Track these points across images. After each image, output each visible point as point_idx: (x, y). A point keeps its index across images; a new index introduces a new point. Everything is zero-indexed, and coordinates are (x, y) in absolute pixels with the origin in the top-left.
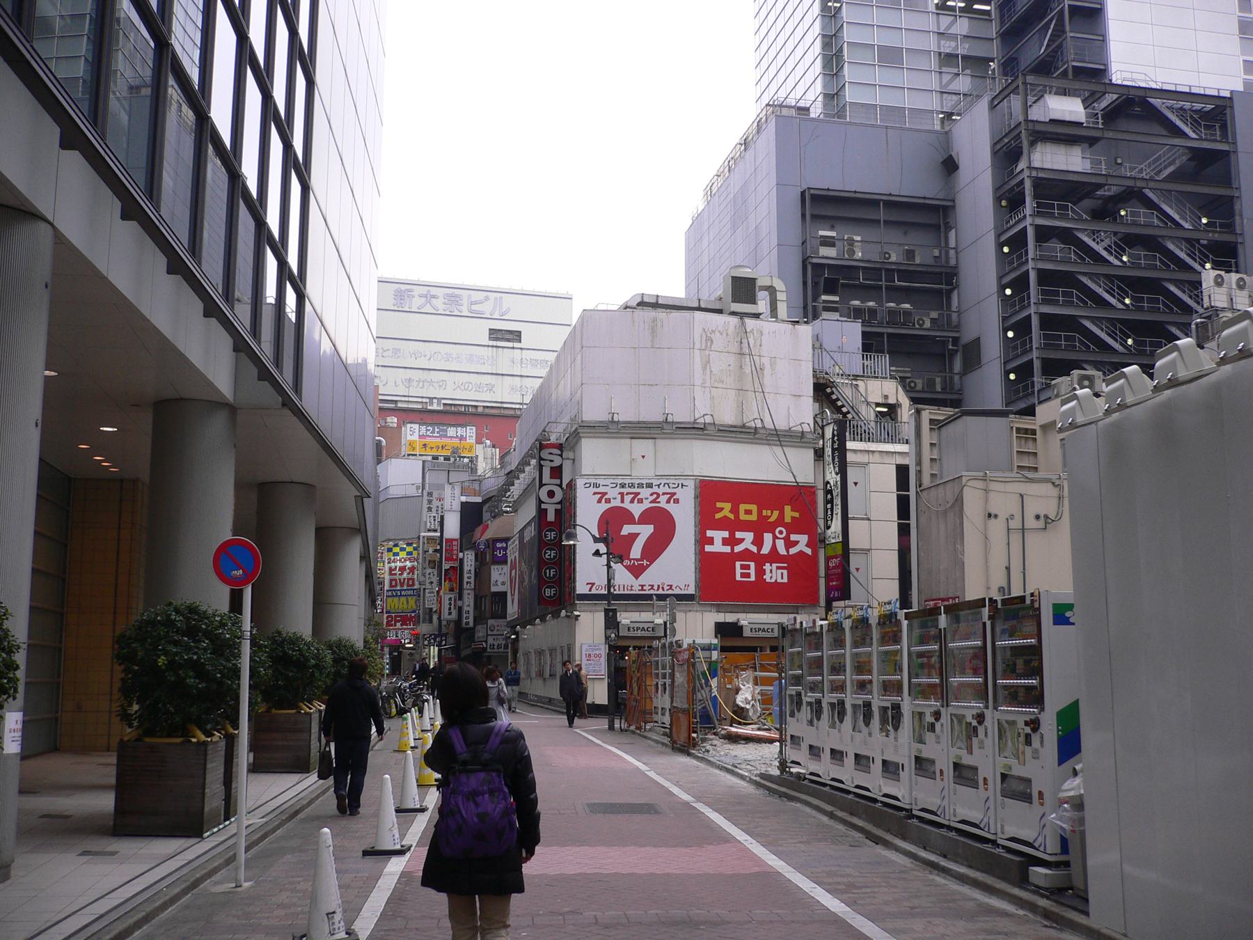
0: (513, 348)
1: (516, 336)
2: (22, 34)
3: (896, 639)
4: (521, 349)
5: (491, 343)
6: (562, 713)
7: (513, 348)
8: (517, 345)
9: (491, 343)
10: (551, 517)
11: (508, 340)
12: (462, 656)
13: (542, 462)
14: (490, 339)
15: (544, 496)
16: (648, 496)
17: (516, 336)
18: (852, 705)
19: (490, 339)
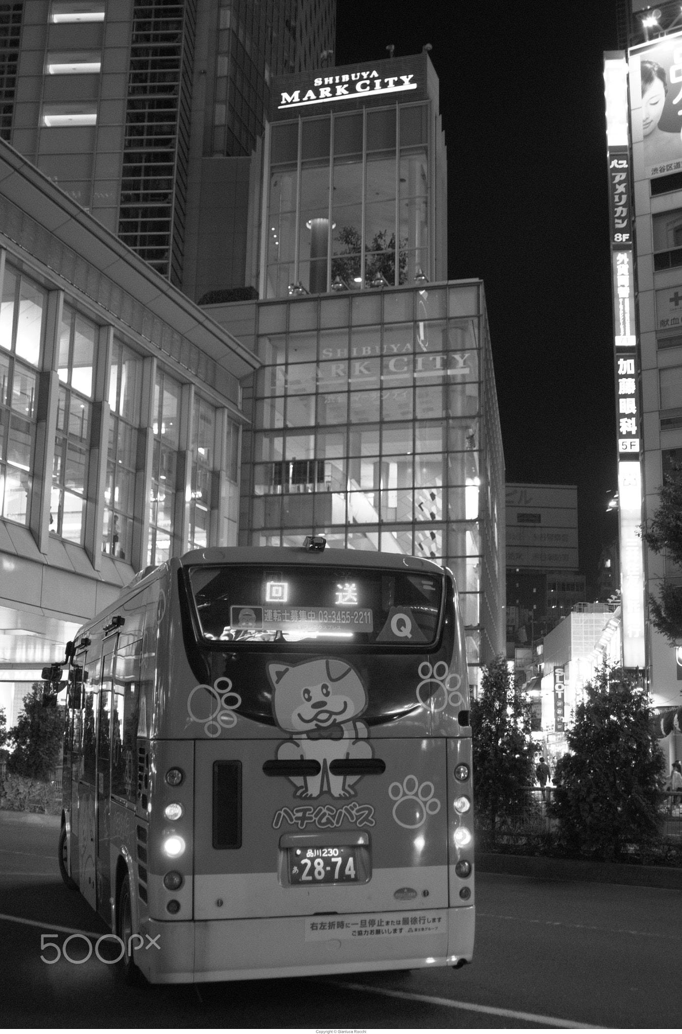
0: (535, 527)
1: (537, 518)
2: (221, 461)
3: (143, 114)
4: (541, 527)
5: (519, 524)
6: (422, 153)
7: (535, 527)
8: (537, 524)
9: (519, 524)
10: (560, 696)
11: (532, 521)
12: (65, 689)
13: (351, 246)
14: (519, 521)
15: (557, 688)
16: (339, 253)
17: (537, 518)
18: (332, 259)
19: (519, 521)
